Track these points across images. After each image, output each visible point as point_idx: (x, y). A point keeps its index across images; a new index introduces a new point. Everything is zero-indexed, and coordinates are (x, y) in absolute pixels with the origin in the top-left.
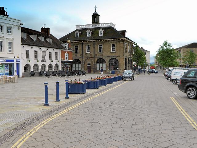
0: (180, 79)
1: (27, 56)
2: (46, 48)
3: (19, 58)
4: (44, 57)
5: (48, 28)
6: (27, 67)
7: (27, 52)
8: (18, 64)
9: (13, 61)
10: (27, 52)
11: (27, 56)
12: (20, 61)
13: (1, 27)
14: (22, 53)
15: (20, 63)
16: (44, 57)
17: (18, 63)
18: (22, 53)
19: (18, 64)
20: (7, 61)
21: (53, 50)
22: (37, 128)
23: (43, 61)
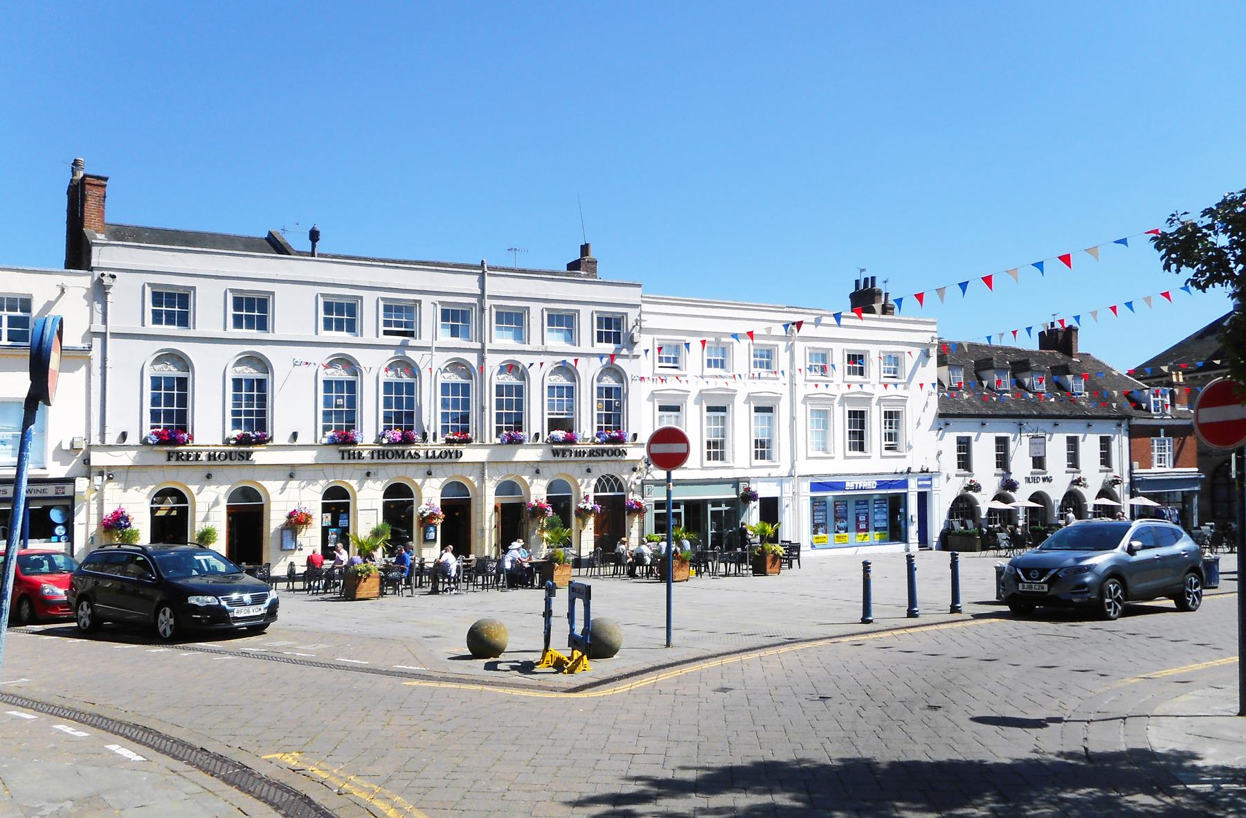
0: (872, 311)
1: (965, 462)
2: (981, 420)
3: (927, 471)
4: (1039, 462)
5: (310, 232)
6: (963, 507)
7: (964, 446)
8: (923, 498)
9: (904, 484)
10: (964, 446)
11: (965, 462)
12: (930, 486)
13: (1, 317)
14: (939, 454)
15: (905, 494)
16: (1039, 462)
17: (925, 493)
18: (939, 454)
19: (923, 498)
20: (881, 485)
21: (1086, 425)
22: (362, 789)
23: (1035, 480)
